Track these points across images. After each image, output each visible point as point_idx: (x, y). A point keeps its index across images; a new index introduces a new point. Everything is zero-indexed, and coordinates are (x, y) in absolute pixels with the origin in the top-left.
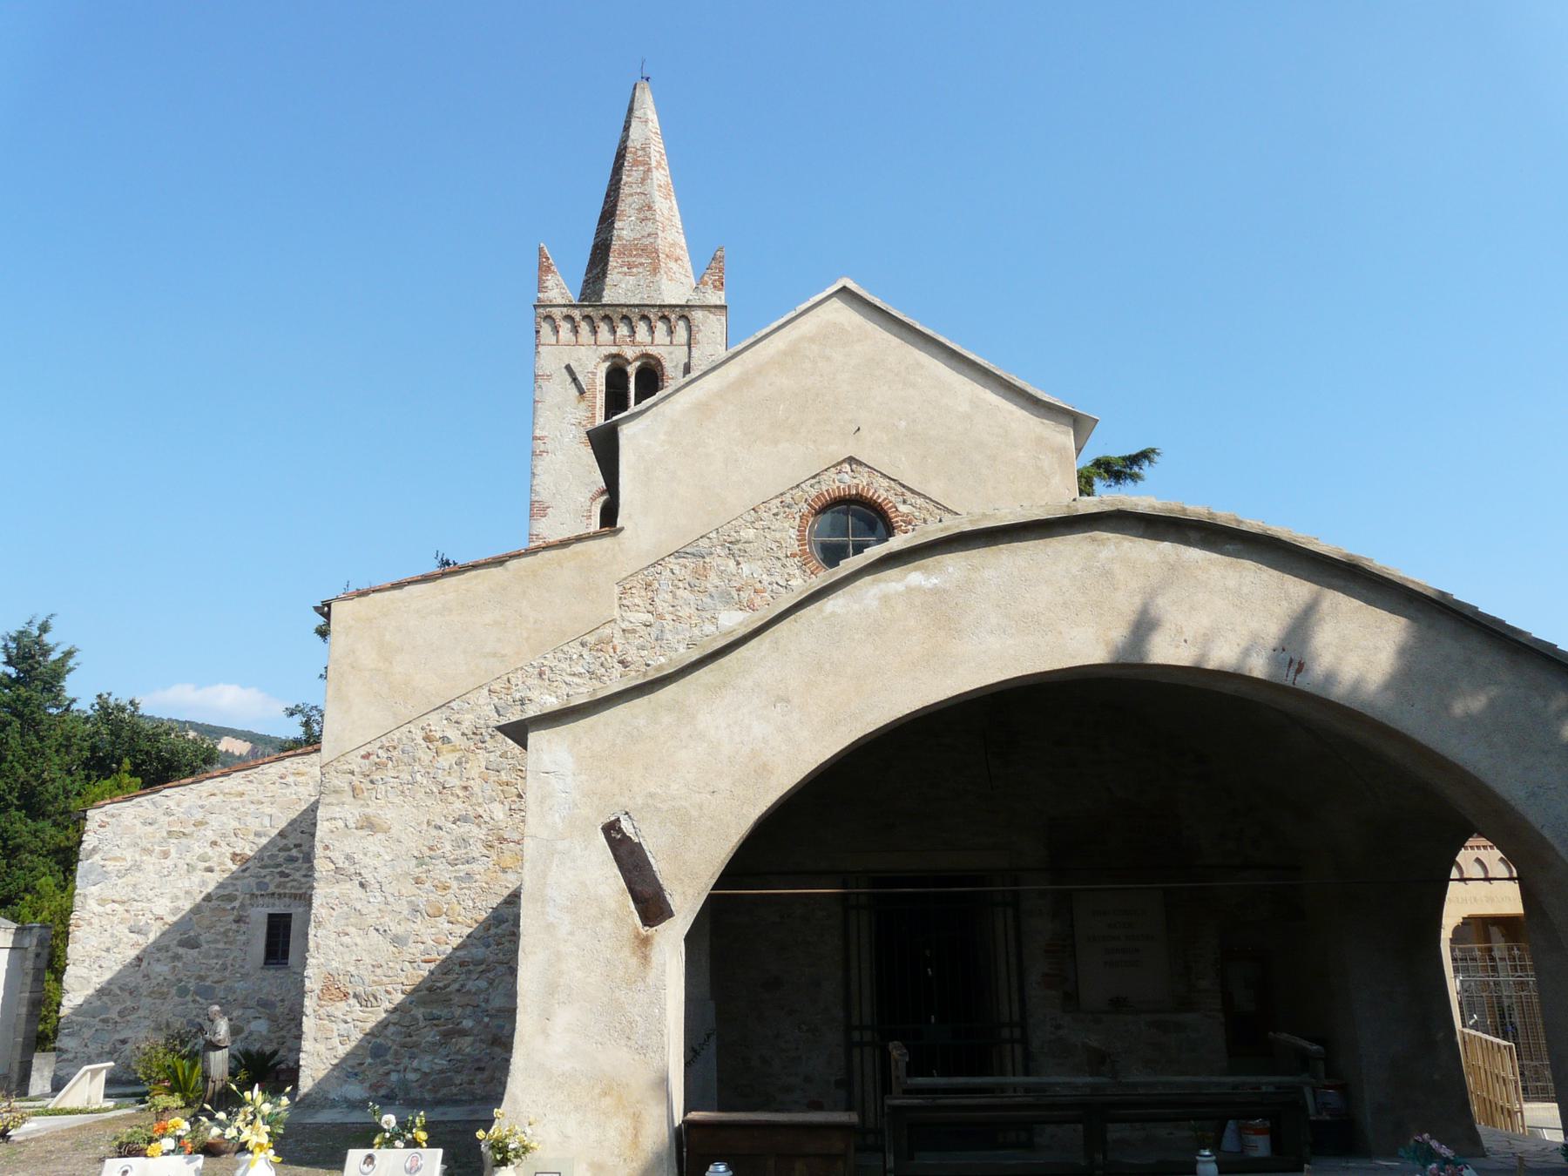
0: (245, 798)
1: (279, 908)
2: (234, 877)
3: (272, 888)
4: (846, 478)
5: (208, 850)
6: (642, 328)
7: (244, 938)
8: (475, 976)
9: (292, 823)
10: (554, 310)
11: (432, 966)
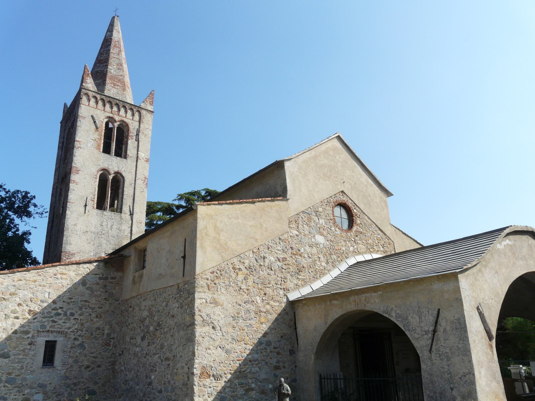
0: (37, 283)
1: (51, 338)
2: (29, 322)
3: (48, 328)
4: (342, 197)
5: (17, 308)
6: (122, 111)
7: (33, 353)
8: (254, 366)
9: (59, 297)
10: (89, 92)
11: (240, 362)
